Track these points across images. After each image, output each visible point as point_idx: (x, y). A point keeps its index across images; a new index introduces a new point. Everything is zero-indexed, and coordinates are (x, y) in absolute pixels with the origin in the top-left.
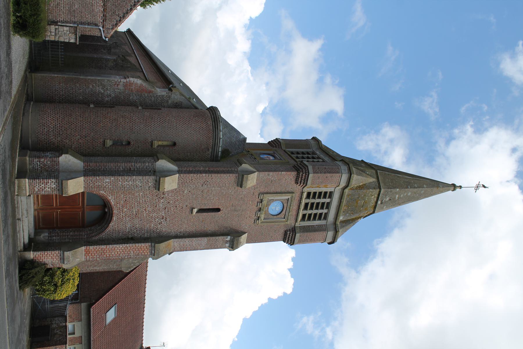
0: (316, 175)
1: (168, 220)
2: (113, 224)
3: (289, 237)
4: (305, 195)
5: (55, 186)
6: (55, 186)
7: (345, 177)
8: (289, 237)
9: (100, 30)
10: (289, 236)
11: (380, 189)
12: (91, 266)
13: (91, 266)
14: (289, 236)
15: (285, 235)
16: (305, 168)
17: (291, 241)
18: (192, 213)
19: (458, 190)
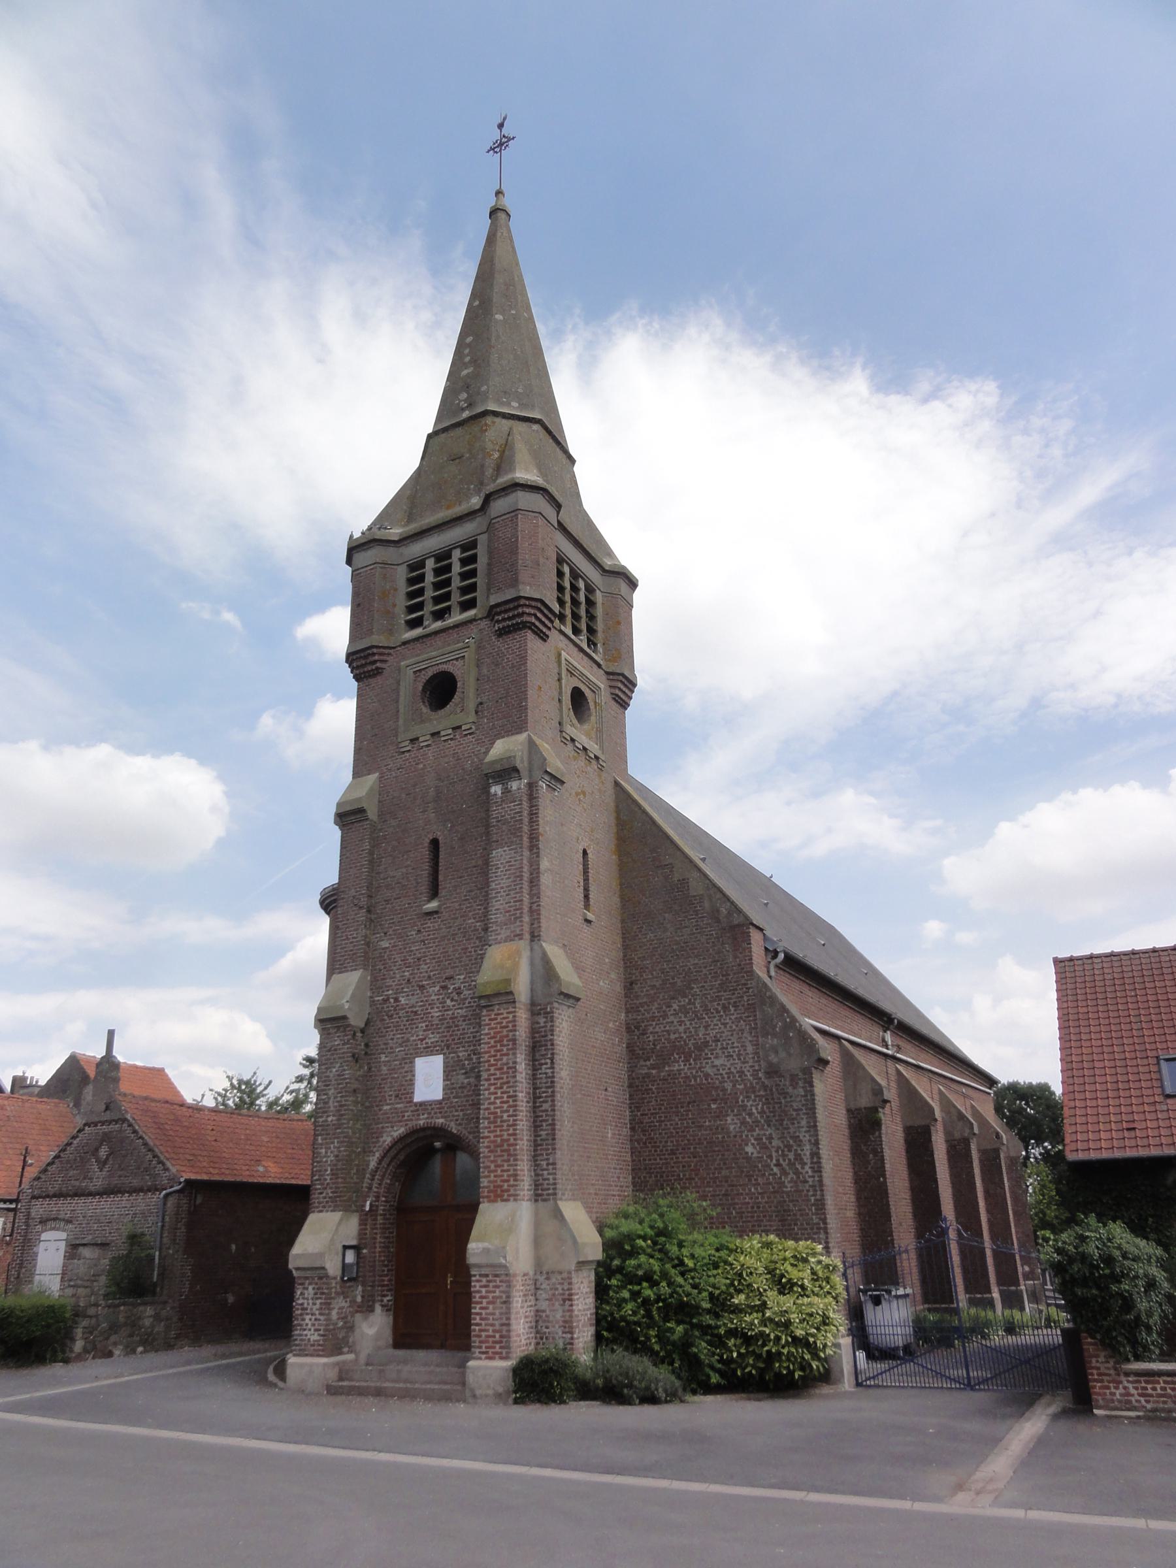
0: (524, 576)
1: (449, 972)
2: (452, 1124)
3: (509, 619)
4: (418, 631)
5: (310, 1288)
6: (310, 1288)
7: (524, 499)
8: (509, 619)
9: (167, 1195)
10: (504, 620)
11: (485, 413)
12: (797, 1173)
13: (797, 1173)
14: (504, 620)
15: (510, 632)
16: (374, 654)
17: (516, 608)
18: (436, 912)
19: (507, 202)
